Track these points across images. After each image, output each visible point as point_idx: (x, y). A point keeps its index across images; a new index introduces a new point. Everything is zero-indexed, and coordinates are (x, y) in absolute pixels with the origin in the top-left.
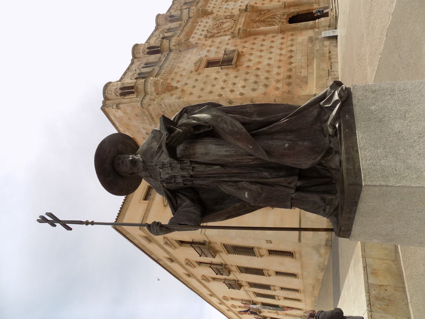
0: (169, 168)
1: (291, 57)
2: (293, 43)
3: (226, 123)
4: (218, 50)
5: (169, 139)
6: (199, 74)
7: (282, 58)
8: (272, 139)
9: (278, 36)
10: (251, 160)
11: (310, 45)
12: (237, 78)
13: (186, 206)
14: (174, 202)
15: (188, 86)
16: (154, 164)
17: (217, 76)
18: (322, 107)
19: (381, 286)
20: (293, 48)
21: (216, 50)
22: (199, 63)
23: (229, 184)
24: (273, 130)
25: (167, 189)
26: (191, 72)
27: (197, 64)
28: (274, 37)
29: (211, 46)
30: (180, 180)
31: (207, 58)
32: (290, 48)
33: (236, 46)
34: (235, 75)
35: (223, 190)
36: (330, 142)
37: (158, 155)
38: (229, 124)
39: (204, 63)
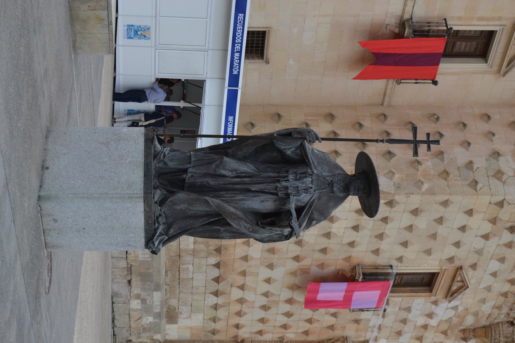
0: (300, 189)
1: (217, 280)
2: (213, 313)
3: (245, 227)
4: (403, 315)
5: (290, 219)
6: (451, 260)
7: (240, 280)
8: (207, 211)
9: (251, 333)
10: (224, 195)
11: (174, 302)
12: (351, 240)
13: (289, 149)
14: (303, 152)
15: (483, 233)
16: (317, 192)
17: (400, 251)
18: (167, 235)
19: (94, 10)
20: (212, 300)
21: (410, 316)
22: (454, 288)
23: (244, 174)
24: (205, 219)
25: (308, 166)
26: (474, 266)
27: (460, 284)
28: (260, 333)
29: (425, 327)
30: (291, 177)
31: (433, 298)
32: (220, 300)
33: (357, 321)
34: (355, 249)
35: (252, 166)
36: (161, 210)
37: (312, 200)
38: (242, 226)
39: (441, 285)
